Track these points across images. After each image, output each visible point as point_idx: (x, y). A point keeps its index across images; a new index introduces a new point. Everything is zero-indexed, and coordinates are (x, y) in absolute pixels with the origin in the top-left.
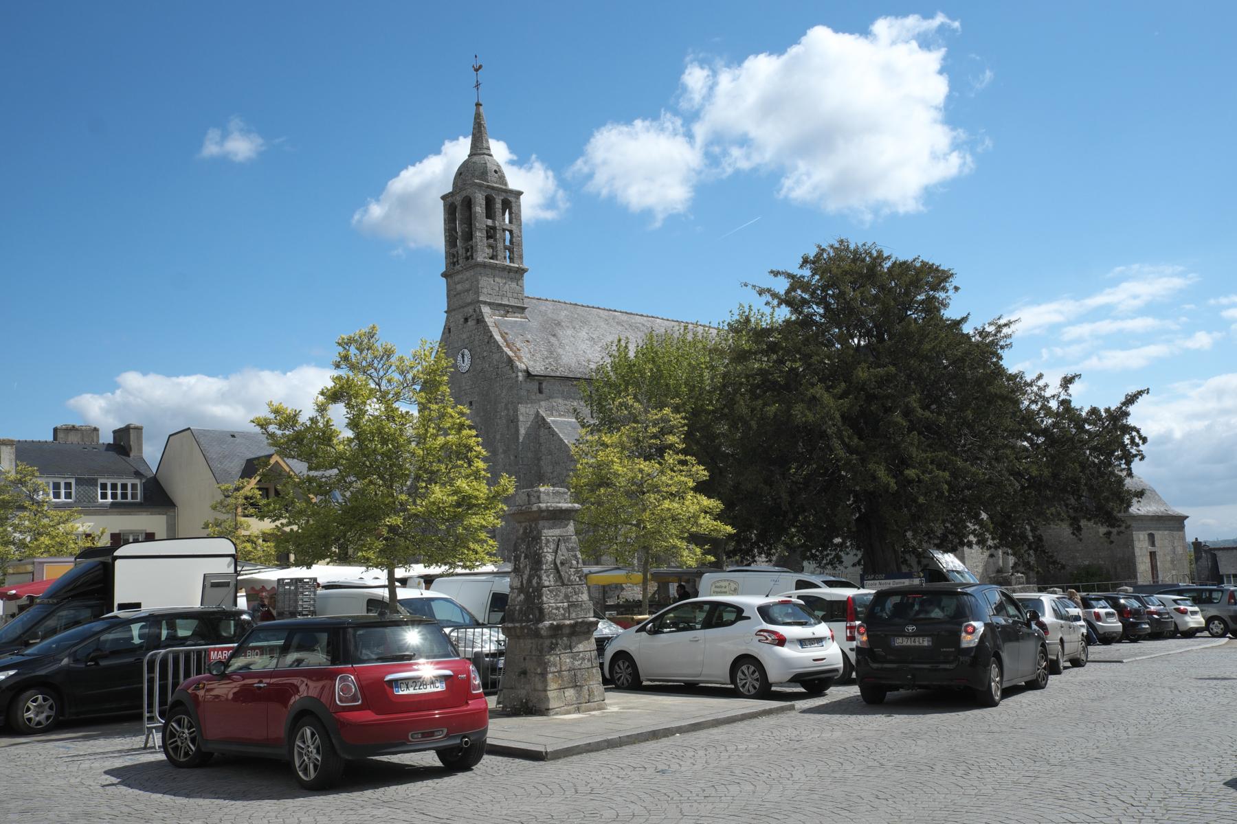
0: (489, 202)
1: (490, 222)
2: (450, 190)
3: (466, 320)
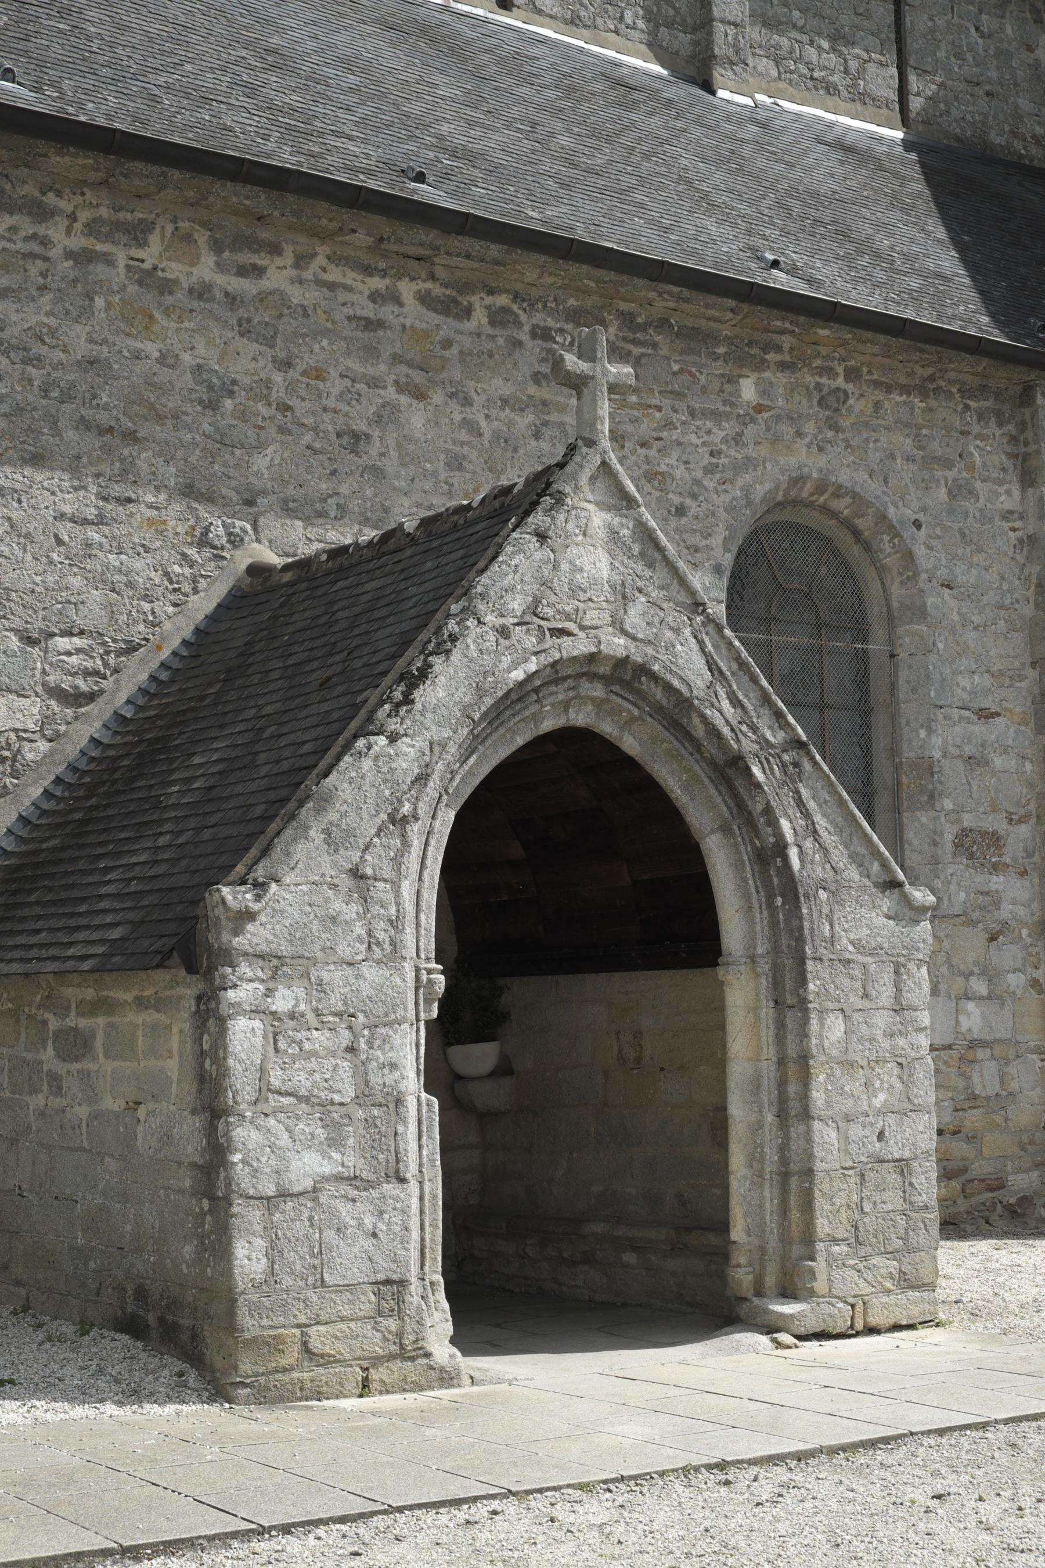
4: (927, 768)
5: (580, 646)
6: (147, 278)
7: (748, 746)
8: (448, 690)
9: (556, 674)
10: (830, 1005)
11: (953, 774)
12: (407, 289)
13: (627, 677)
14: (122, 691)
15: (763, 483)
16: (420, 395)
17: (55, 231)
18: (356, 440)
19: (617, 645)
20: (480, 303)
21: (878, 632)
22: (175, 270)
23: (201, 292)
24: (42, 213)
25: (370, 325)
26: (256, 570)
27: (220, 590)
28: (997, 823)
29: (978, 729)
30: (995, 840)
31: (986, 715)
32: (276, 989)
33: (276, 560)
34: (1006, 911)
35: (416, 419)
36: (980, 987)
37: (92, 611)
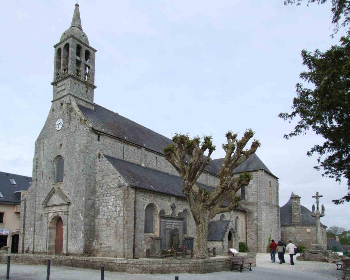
0: (79, 48)
1: (78, 58)
2: (224, 157)
3: (62, 104)
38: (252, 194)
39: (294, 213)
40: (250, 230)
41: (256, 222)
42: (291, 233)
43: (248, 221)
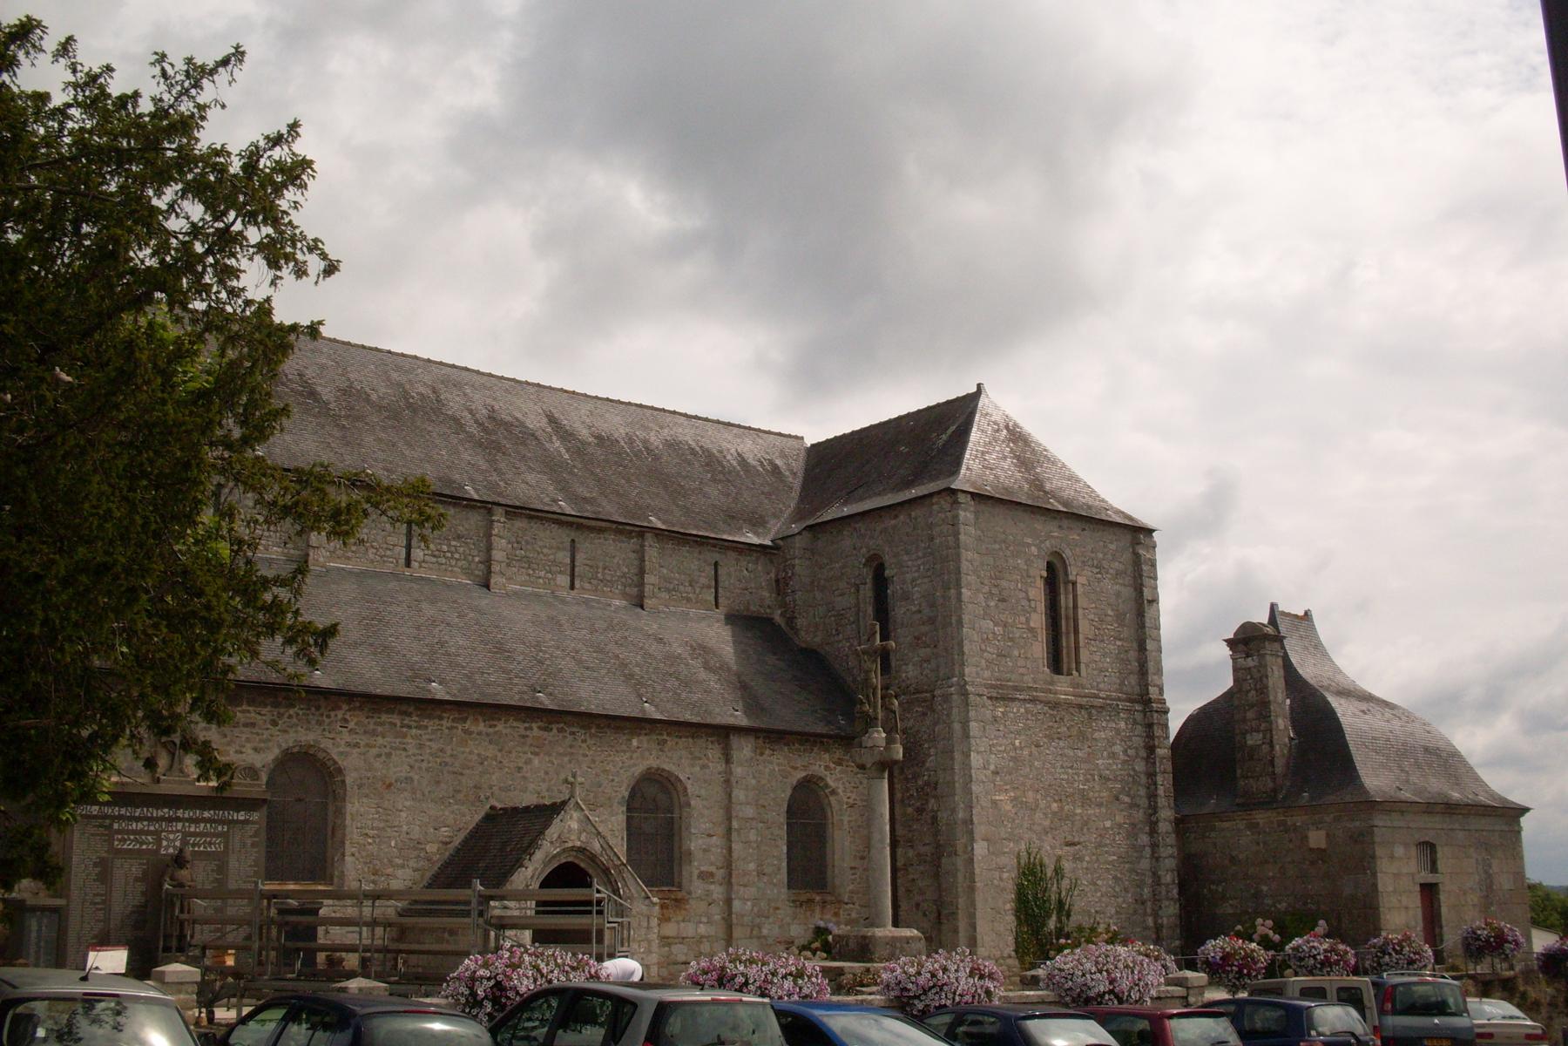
4: (690, 853)
5: (570, 844)
6: (466, 731)
7: (610, 865)
8: (539, 855)
9: (564, 850)
10: (816, 945)
11: (698, 855)
12: (534, 726)
13: (582, 850)
14: (457, 841)
15: (639, 769)
16: (537, 754)
17: (444, 722)
18: (520, 769)
19: (578, 844)
20: (554, 727)
21: (677, 810)
22: (473, 728)
23: (480, 733)
24: (441, 718)
25: (524, 737)
26: (492, 808)
27: (483, 814)
28: (713, 869)
29: (708, 840)
30: (712, 875)
31: (710, 836)
32: (1370, 830)
33: (499, 806)
34: (715, 896)
35: (536, 761)
36: (704, 919)
37: (450, 821)
38: (917, 638)
39: (1244, 734)
40: (911, 853)
41: (932, 803)
42: (1233, 860)
43: (902, 801)
